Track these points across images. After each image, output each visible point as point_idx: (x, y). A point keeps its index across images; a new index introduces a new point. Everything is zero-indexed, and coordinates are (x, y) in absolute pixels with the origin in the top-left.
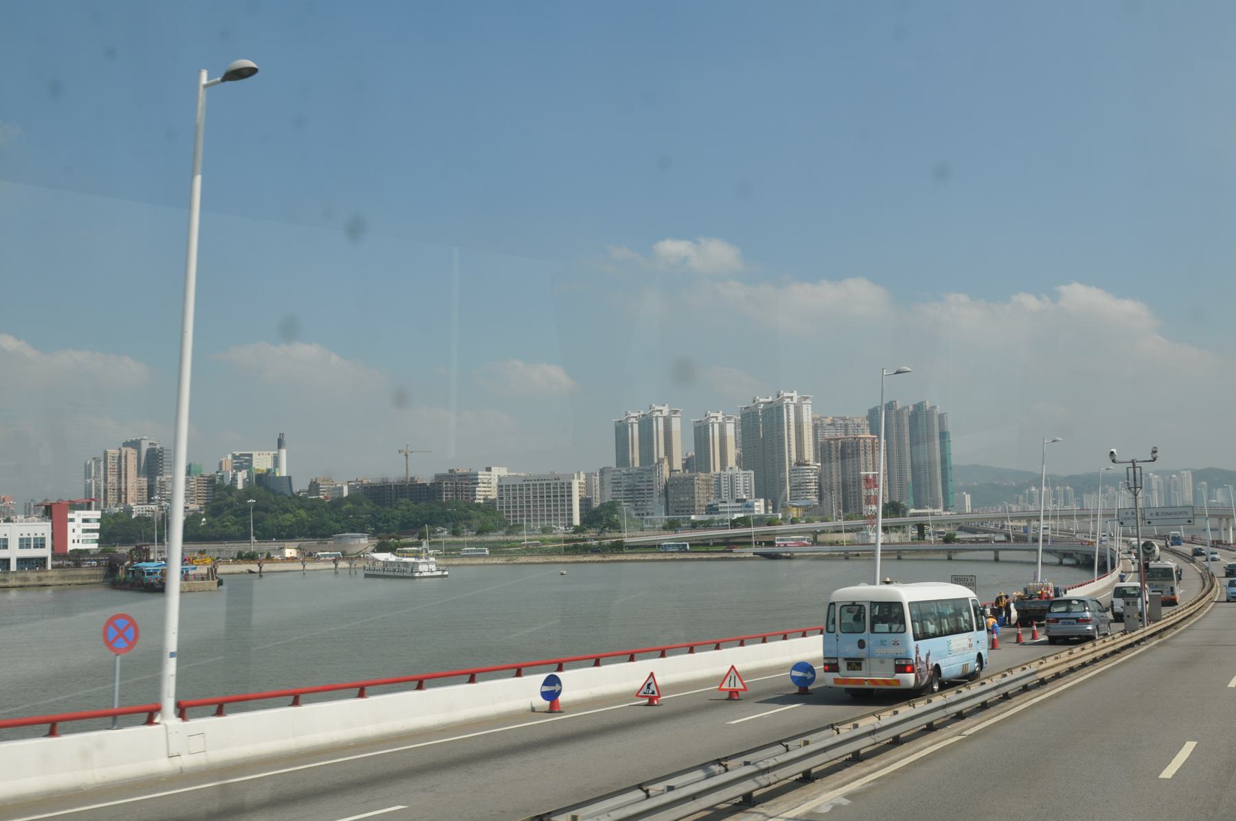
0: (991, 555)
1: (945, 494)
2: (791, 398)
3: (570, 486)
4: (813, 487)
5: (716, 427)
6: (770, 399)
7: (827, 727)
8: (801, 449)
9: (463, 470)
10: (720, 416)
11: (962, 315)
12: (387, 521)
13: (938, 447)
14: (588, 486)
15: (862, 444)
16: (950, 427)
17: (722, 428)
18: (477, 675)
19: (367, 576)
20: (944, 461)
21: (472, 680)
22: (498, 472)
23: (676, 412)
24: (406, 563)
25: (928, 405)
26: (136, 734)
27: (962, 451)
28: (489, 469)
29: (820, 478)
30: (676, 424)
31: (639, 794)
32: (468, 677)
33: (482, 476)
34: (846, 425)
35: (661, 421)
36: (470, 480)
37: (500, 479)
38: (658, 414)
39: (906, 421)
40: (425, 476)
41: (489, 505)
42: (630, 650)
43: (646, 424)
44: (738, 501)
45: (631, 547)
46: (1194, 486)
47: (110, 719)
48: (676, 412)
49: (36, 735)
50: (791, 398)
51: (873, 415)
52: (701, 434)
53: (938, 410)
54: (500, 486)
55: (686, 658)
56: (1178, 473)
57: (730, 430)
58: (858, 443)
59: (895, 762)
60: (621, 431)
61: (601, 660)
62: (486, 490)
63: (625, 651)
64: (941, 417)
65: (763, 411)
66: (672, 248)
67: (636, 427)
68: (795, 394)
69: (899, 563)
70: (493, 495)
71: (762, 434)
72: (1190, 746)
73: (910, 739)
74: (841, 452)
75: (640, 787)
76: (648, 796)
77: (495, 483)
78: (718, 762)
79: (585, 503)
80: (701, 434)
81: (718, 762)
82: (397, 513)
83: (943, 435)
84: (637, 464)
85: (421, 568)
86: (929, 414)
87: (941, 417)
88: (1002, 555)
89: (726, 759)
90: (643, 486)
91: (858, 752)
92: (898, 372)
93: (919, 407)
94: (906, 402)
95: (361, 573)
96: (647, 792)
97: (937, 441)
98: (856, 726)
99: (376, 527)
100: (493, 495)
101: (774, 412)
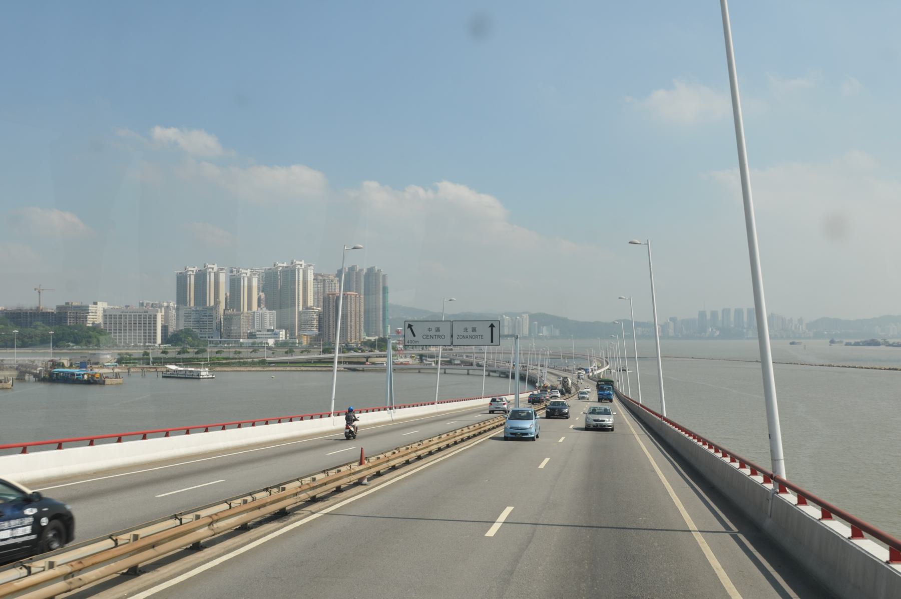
0: (466, 372)
3: (155, 317)
4: (315, 323)
6: (285, 265)
7: (264, 490)
8: (307, 297)
9: (84, 304)
10: (248, 272)
11: (376, 194)
12: (32, 337)
13: (381, 297)
14: (166, 318)
16: (389, 284)
18: (63, 444)
19: (163, 377)
20: (384, 302)
21: (60, 447)
22: (102, 306)
23: (222, 269)
24: (191, 371)
27: (393, 298)
28: (95, 303)
29: (320, 318)
31: (109, 543)
32: (89, 442)
33: (92, 308)
34: (324, 280)
36: (82, 312)
37: (105, 311)
39: (362, 279)
40: (50, 305)
41: (95, 327)
42: (206, 425)
43: (201, 277)
44: (268, 331)
45: (270, 363)
46: (530, 324)
51: (339, 274)
52: (235, 284)
54: (105, 316)
55: (250, 429)
56: (520, 315)
59: (379, 485)
60: (182, 280)
61: (95, 441)
62: (96, 316)
63: (55, 439)
64: (384, 276)
67: (193, 277)
68: (302, 262)
69: (420, 375)
70: (99, 320)
71: (278, 289)
72: (547, 460)
73: (322, 499)
75: (175, 517)
76: (30, 573)
77: (100, 313)
78: (277, 486)
79: (165, 328)
80: (235, 284)
81: (277, 486)
82: (38, 332)
83: (385, 289)
84: (192, 304)
85: (202, 374)
86: (377, 275)
87: (384, 276)
88: (471, 372)
89: (302, 478)
90: (206, 319)
91: (284, 508)
92: (355, 248)
93: (370, 270)
94: (363, 266)
95: (160, 375)
96: (116, 541)
98: (284, 489)
99: (23, 341)
100: (99, 320)
101: (290, 273)
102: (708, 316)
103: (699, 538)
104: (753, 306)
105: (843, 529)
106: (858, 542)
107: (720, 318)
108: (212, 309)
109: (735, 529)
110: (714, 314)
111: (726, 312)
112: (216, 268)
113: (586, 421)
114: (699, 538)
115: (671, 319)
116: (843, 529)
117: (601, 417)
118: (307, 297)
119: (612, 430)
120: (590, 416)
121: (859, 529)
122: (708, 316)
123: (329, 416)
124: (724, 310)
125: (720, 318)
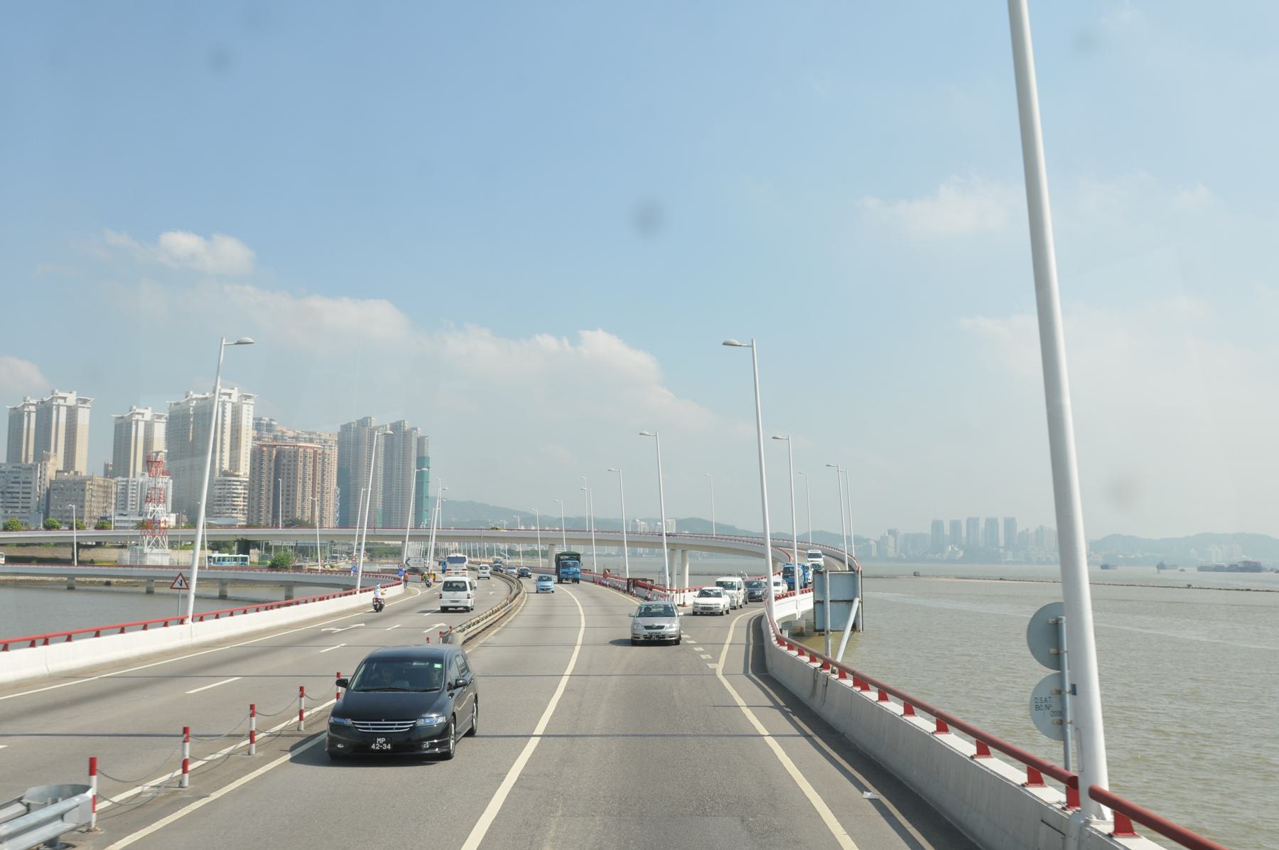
1: (321, 521)
2: (230, 395)
5: (141, 426)
15: (301, 454)
16: (431, 452)
17: (149, 427)
23: (85, 401)
25: (407, 426)
26: (174, 629)
30: (83, 417)
35: (63, 411)
38: (61, 402)
43: (45, 411)
47: (340, 591)
48: (85, 401)
49: (24, 647)
50: (230, 395)
52: (123, 431)
53: (420, 432)
57: (160, 431)
58: (296, 453)
60: (16, 418)
64: (421, 441)
65: (195, 408)
66: (182, 242)
67: (33, 416)
74: (277, 466)
83: (422, 461)
86: (407, 435)
90: (18, 488)
93: (396, 426)
97: (414, 464)
101: (204, 414)
102: (947, 529)
103: (771, 741)
104: (1052, 524)
105: (925, 723)
106: (942, 737)
107: (964, 534)
108: (31, 469)
109: (809, 732)
110: (955, 526)
111: (972, 522)
112: (148, 414)
113: (633, 629)
114: (771, 741)
115: (890, 532)
116: (925, 723)
117: (657, 622)
118: (232, 458)
119: (677, 642)
120: (640, 620)
121: (944, 723)
122: (947, 529)
123: (182, 622)
124: (969, 520)
125: (964, 534)
